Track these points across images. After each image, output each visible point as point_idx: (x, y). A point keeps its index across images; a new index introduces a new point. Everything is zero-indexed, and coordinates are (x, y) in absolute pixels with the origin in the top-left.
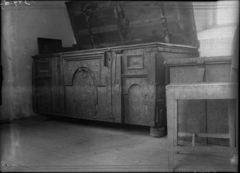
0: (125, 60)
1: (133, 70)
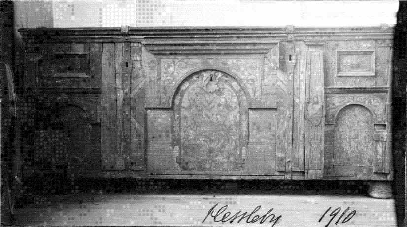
0: (333, 60)
1: (348, 79)
